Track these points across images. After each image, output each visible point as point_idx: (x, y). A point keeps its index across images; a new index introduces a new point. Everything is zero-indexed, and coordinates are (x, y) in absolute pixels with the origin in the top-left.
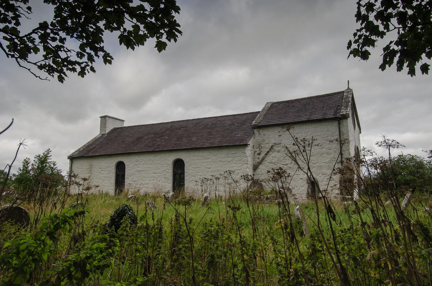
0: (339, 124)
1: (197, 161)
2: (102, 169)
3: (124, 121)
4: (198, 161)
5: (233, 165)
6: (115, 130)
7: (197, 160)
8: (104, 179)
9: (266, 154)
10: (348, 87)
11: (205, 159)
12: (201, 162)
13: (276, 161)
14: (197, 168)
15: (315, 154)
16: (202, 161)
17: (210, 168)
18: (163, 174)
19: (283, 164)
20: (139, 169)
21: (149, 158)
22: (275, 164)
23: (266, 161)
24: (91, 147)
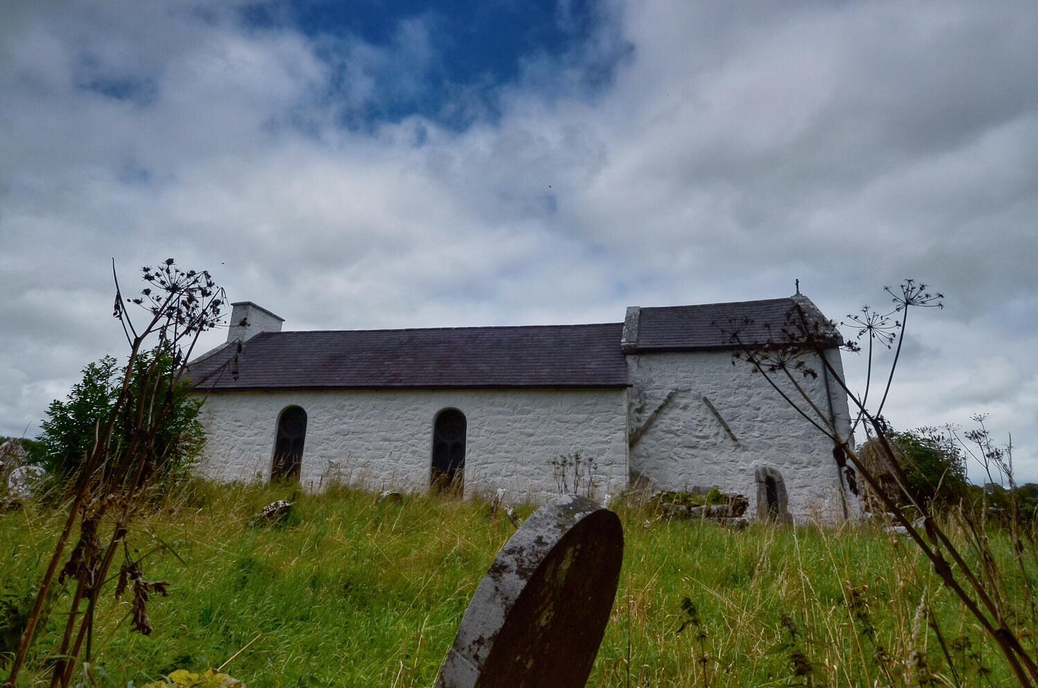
1: (500, 417)
2: (239, 424)
3: (284, 320)
4: (504, 417)
5: (591, 430)
6: (264, 336)
7: (500, 413)
8: (244, 447)
9: (657, 412)
10: (798, 292)
11: (520, 413)
12: (509, 420)
13: (681, 427)
14: (499, 432)
15: (771, 418)
16: (511, 418)
17: (532, 435)
18: (409, 442)
20: (345, 427)
21: (374, 402)
22: (678, 435)
23: (656, 426)
24: (210, 369)
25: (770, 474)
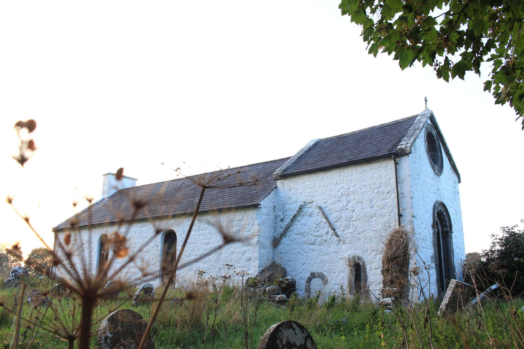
0: (396, 164)
10: (426, 108)
16: (198, 233)
17: (208, 244)
19: (316, 236)
23: (292, 231)
25: (357, 261)
